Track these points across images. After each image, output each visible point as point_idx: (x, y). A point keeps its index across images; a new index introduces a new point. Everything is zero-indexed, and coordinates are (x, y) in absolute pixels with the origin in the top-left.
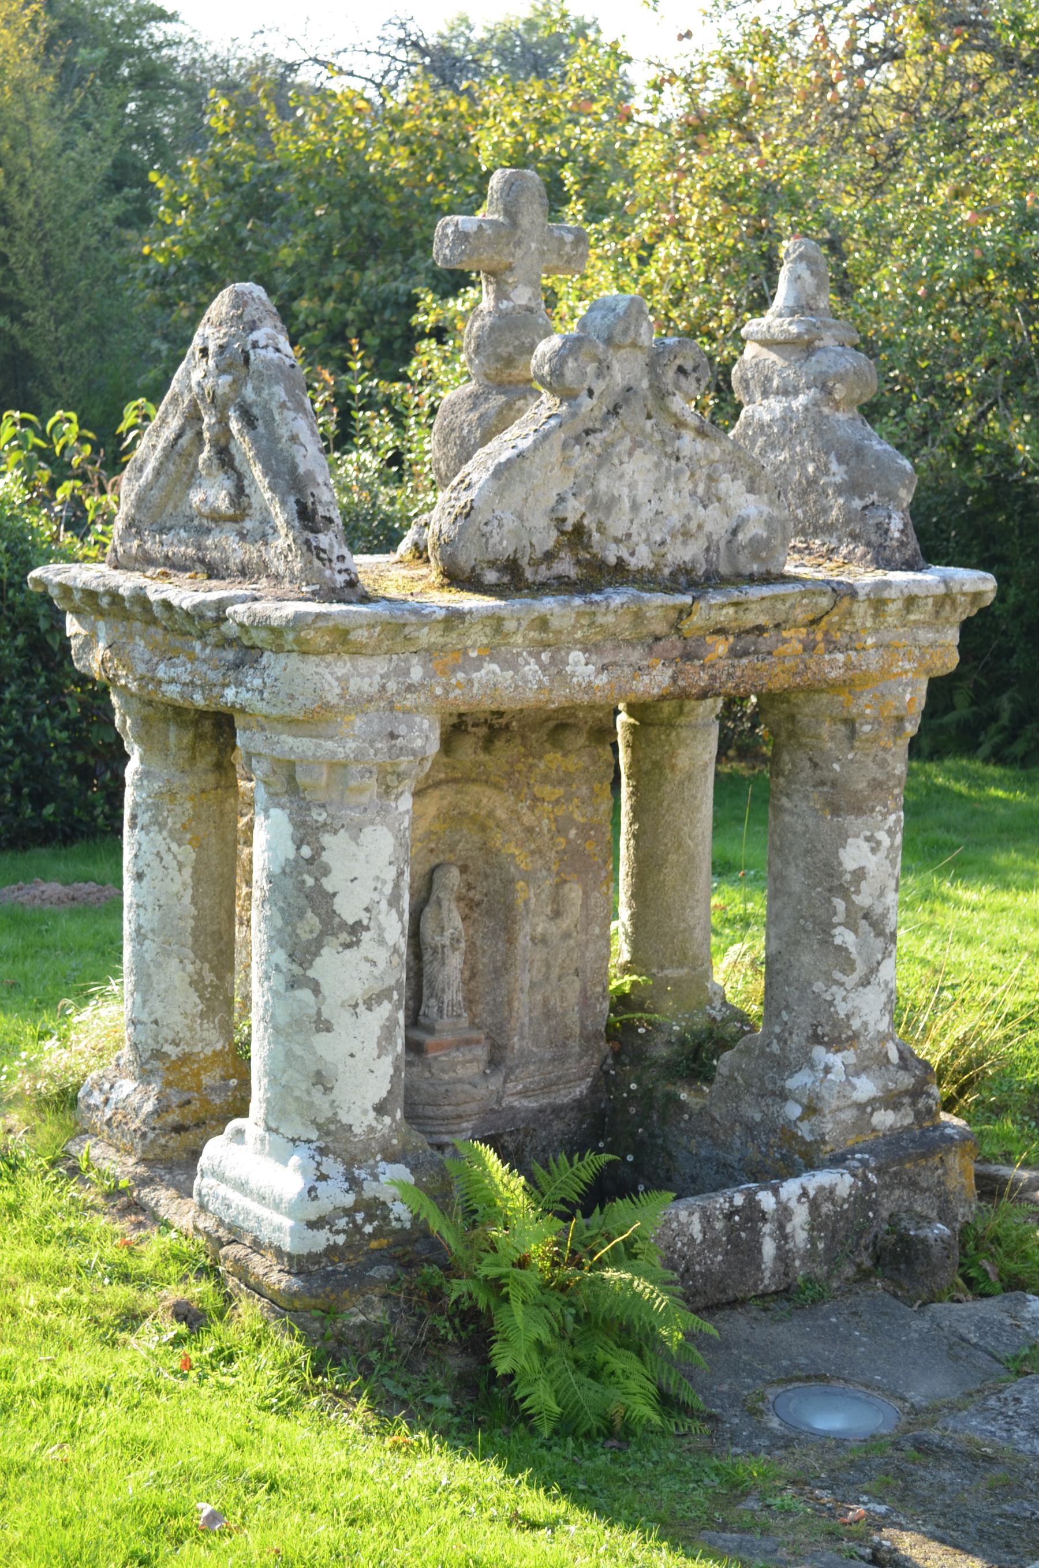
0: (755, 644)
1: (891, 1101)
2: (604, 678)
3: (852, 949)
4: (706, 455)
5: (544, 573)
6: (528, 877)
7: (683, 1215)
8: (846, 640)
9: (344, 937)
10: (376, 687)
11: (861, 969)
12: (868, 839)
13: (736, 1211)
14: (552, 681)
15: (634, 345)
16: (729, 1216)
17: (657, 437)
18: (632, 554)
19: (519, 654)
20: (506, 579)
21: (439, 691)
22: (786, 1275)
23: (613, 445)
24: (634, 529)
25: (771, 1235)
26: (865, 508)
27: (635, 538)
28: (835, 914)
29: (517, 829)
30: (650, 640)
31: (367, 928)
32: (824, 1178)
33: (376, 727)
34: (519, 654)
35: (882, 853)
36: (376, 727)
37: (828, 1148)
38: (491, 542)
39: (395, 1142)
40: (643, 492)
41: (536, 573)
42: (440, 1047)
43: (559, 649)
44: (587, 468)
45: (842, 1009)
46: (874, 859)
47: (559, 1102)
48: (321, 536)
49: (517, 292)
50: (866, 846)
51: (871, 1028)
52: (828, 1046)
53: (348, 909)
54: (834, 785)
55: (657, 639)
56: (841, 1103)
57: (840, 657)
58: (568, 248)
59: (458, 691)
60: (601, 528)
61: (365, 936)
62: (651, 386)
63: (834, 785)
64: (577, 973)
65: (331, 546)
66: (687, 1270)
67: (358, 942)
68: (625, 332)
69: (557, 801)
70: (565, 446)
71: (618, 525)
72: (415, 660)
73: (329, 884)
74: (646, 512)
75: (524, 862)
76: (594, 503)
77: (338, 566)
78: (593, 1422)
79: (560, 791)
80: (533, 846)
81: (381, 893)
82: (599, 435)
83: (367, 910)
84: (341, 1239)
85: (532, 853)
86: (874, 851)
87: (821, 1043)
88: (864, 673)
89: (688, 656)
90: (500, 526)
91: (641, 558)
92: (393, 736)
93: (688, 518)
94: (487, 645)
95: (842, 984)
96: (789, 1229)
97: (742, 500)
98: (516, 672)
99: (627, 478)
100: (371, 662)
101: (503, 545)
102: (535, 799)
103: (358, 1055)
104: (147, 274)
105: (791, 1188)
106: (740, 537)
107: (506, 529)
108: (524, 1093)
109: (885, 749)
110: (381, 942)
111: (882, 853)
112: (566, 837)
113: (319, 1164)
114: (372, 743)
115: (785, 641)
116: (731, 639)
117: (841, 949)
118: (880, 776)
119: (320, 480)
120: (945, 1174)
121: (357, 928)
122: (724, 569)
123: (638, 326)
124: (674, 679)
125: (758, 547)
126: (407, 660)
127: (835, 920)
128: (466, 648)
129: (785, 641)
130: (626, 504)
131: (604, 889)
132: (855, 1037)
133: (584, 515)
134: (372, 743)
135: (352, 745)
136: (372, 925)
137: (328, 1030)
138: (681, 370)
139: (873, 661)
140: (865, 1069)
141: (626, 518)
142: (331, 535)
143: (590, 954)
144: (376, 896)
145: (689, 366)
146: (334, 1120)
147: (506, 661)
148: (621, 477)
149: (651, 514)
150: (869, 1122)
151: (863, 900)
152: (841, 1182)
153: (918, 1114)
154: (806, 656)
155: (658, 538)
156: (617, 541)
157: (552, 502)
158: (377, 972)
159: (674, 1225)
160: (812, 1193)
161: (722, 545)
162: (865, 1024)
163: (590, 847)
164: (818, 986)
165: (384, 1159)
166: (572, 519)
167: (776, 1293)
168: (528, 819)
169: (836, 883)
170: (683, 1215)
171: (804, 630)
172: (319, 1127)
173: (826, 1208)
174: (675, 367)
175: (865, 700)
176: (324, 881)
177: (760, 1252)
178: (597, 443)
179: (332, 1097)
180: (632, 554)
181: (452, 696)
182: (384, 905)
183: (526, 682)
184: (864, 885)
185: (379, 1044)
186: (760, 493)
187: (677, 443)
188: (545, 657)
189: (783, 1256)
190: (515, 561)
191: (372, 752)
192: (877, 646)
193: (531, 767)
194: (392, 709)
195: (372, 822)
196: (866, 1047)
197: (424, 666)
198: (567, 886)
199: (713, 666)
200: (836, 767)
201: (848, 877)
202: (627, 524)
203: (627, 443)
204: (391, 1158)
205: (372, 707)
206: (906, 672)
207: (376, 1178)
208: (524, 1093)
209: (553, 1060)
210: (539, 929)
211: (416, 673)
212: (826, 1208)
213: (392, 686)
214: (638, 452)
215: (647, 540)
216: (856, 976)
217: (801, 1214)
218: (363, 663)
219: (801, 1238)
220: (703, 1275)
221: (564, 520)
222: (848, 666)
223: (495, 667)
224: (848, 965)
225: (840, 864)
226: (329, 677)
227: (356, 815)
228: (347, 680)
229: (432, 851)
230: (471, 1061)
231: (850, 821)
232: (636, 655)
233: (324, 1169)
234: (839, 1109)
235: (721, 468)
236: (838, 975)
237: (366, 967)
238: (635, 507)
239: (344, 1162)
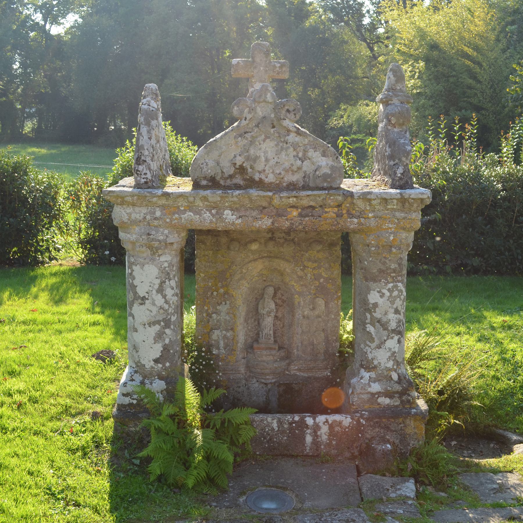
0: (312, 212)
1: (389, 394)
2: (240, 221)
3: (373, 334)
4: (302, 143)
5: (229, 182)
6: (300, 294)
7: (269, 419)
8: (359, 214)
9: (140, 301)
10: (142, 217)
11: (377, 342)
12: (378, 292)
13: (295, 422)
14: (217, 220)
15: (265, 101)
16: (291, 424)
17: (277, 135)
18: (267, 177)
19: (202, 210)
20: (210, 184)
21: (168, 220)
22: (317, 450)
23: (257, 137)
24: (267, 168)
25: (310, 434)
26: (394, 165)
27: (267, 172)
28: (367, 319)
29: (295, 276)
30: (261, 208)
31: (148, 299)
32: (337, 417)
33: (143, 231)
34: (202, 210)
35: (386, 298)
36: (143, 231)
37: (354, 407)
38: (203, 170)
39: (164, 373)
40: (270, 155)
41: (225, 182)
42: (259, 348)
43: (220, 209)
44: (244, 145)
45: (370, 356)
46: (382, 300)
47: (317, 376)
48: (140, 166)
49: (256, 85)
50: (378, 295)
51: (382, 365)
52: (365, 369)
53: (141, 292)
54: (365, 270)
55: (264, 208)
56: (363, 391)
57: (356, 220)
58: (278, 69)
59: (176, 221)
60: (252, 167)
61: (147, 302)
62: (275, 116)
63: (365, 270)
64: (323, 330)
65: (143, 170)
66: (270, 439)
67: (144, 303)
68: (260, 96)
69: (314, 268)
70: (235, 137)
71: (260, 166)
72: (158, 209)
73: (136, 282)
74: (272, 162)
75: (298, 288)
76: (248, 159)
77: (143, 176)
78: (171, 481)
79: (316, 265)
80: (302, 283)
81: (153, 288)
82: (250, 134)
83: (147, 293)
84: (135, 402)
85: (302, 285)
86: (381, 297)
87: (363, 368)
88: (368, 227)
89: (279, 215)
90: (207, 165)
91: (271, 178)
92: (149, 234)
93: (292, 165)
94: (187, 206)
95: (370, 346)
96: (319, 433)
97: (320, 159)
98: (200, 216)
99: (263, 149)
100: (140, 209)
101: (210, 172)
102: (305, 266)
103: (146, 341)
104: (512, 98)
105: (321, 419)
106: (317, 173)
107: (209, 166)
108: (299, 370)
109: (385, 258)
110: (154, 304)
111: (386, 298)
112: (319, 282)
113: (132, 375)
114: (141, 236)
115: (326, 212)
116: (300, 210)
117: (369, 333)
118: (383, 268)
119: (145, 148)
120: (405, 426)
121: (144, 299)
122: (311, 185)
123: (266, 95)
124: (273, 223)
125: (325, 177)
126: (154, 209)
127: (367, 321)
128: (179, 206)
129: (326, 212)
130: (263, 159)
131: (336, 302)
132: (375, 367)
133: (244, 162)
134: (141, 236)
135: (134, 236)
136: (149, 298)
137: (137, 331)
138: (288, 111)
139: (373, 223)
140: (379, 380)
141: (263, 164)
142: (144, 166)
143: (330, 325)
144: (151, 289)
145: (291, 109)
146: (139, 362)
147: (196, 212)
148: (260, 149)
149: (274, 163)
150: (376, 401)
151: (377, 315)
152: (346, 420)
153: (402, 402)
154: (338, 219)
155: (278, 172)
156: (260, 172)
157: (232, 157)
158: (152, 314)
159: (265, 422)
160: (330, 422)
161: (311, 175)
162: (380, 363)
163: (329, 286)
164: (362, 346)
165: (158, 378)
166: (238, 163)
167: (311, 456)
168: (300, 273)
169: (367, 307)
170: (269, 419)
171: (336, 209)
172: (136, 363)
173: (337, 429)
174: (285, 110)
175: (371, 238)
176: (134, 281)
177: (304, 439)
178: (248, 137)
179: (138, 354)
180: (267, 177)
181: (173, 222)
182: (154, 292)
183: (205, 220)
184: (377, 309)
185: (154, 339)
186: (328, 157)
187: (287, 137)
188: (213, 211)
189: (316, 443)
190: (214, 177)
191: (141, 239)
192: (374, 217)
193: (302, 255)
194: (149, 225)
195: (148, 263)
196: (380, 372)
197: (161, 211)
198: (317, 299)
199: (292, 220)
200: (366, 263)
201: (371, 305)
202: (263, 166)
203: (263, 137)
204: (161, 378)
205: (141, 224)
206: (391, 228)
207: (151, 383)
208: (299, 370)
209: (311, 360)
210: (306, 313)
211: (158, 214)
212: (337, 429)
213: (148, 217)
214: (268, 140)
215: (273, 172)
216: (373, 345)
217: (324, 429)
218: (137, 209)
219: (325, 438)
220: (278, 443)
221: (236, 164)
222: (360, 224)
223: (191, 214)
224: (372, 340)
225: (368, 300)
226: (124, 213)
227: (142, 260)
228: (131, 214)
229: (265, 281)
230: (269, 355)
231: (372, 284)
232: (255, 213)
233: (133, 378)
234: (361, 393)
235: (309, 147)
236: (368, 343)
237: (148, 312)
238: (267, 160)
239: (142, 377)
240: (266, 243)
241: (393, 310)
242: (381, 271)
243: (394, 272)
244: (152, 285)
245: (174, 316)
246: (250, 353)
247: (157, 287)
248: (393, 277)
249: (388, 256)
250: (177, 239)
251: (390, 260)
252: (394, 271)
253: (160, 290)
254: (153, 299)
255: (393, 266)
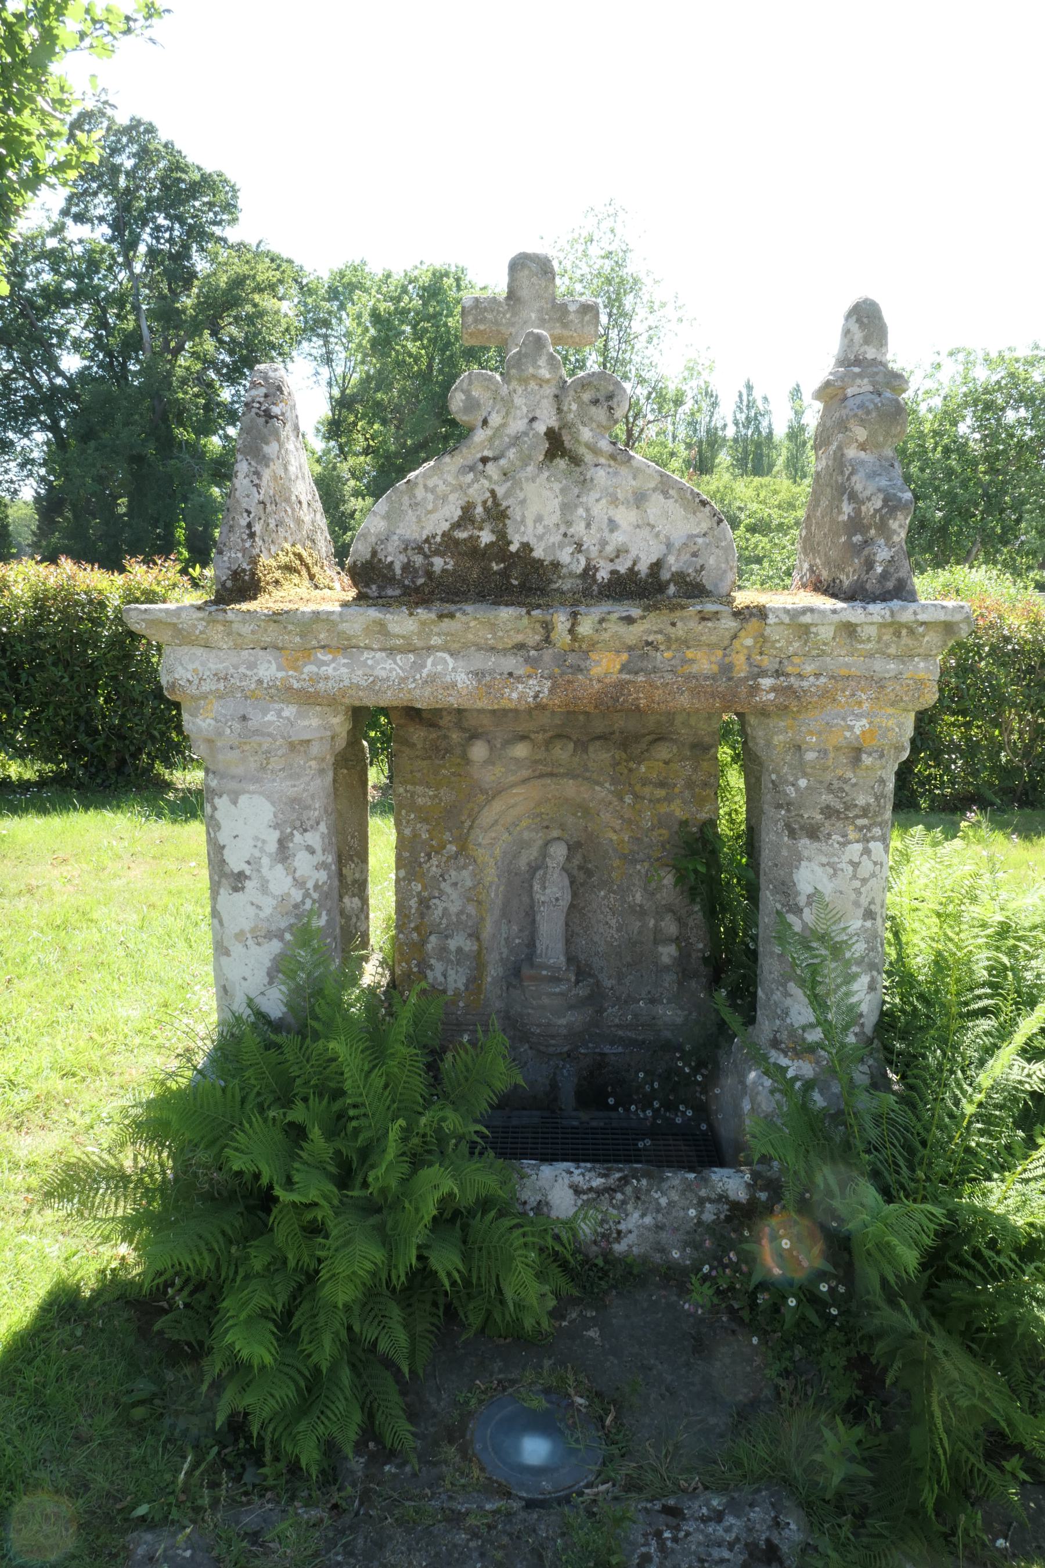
67: (243, 888)
81: (262, 850)
83: (248, 863)
92: (244, 718)
121: (241, 876)
158: (262, 915)
164: (777, 996)
182: (265, 861)
237: (252, 911)
240: (548, 743)
241: (860, 912)
242: (829, 812)
243: (865, 815)
244: (259, 844)
245: (319, 916)
246: (515, 987)
247: (272, 847)
248: (860, 829)
249: (849, 774)
250: (321, 728)
251: (854, 785)
252: (865, 812)
253: (283, 852)
254: (262, 878)
255: (861, 800)
